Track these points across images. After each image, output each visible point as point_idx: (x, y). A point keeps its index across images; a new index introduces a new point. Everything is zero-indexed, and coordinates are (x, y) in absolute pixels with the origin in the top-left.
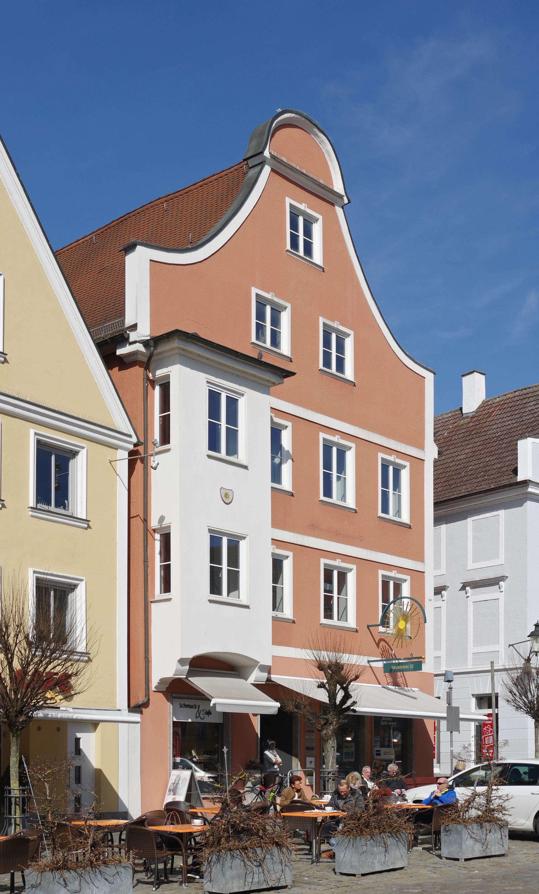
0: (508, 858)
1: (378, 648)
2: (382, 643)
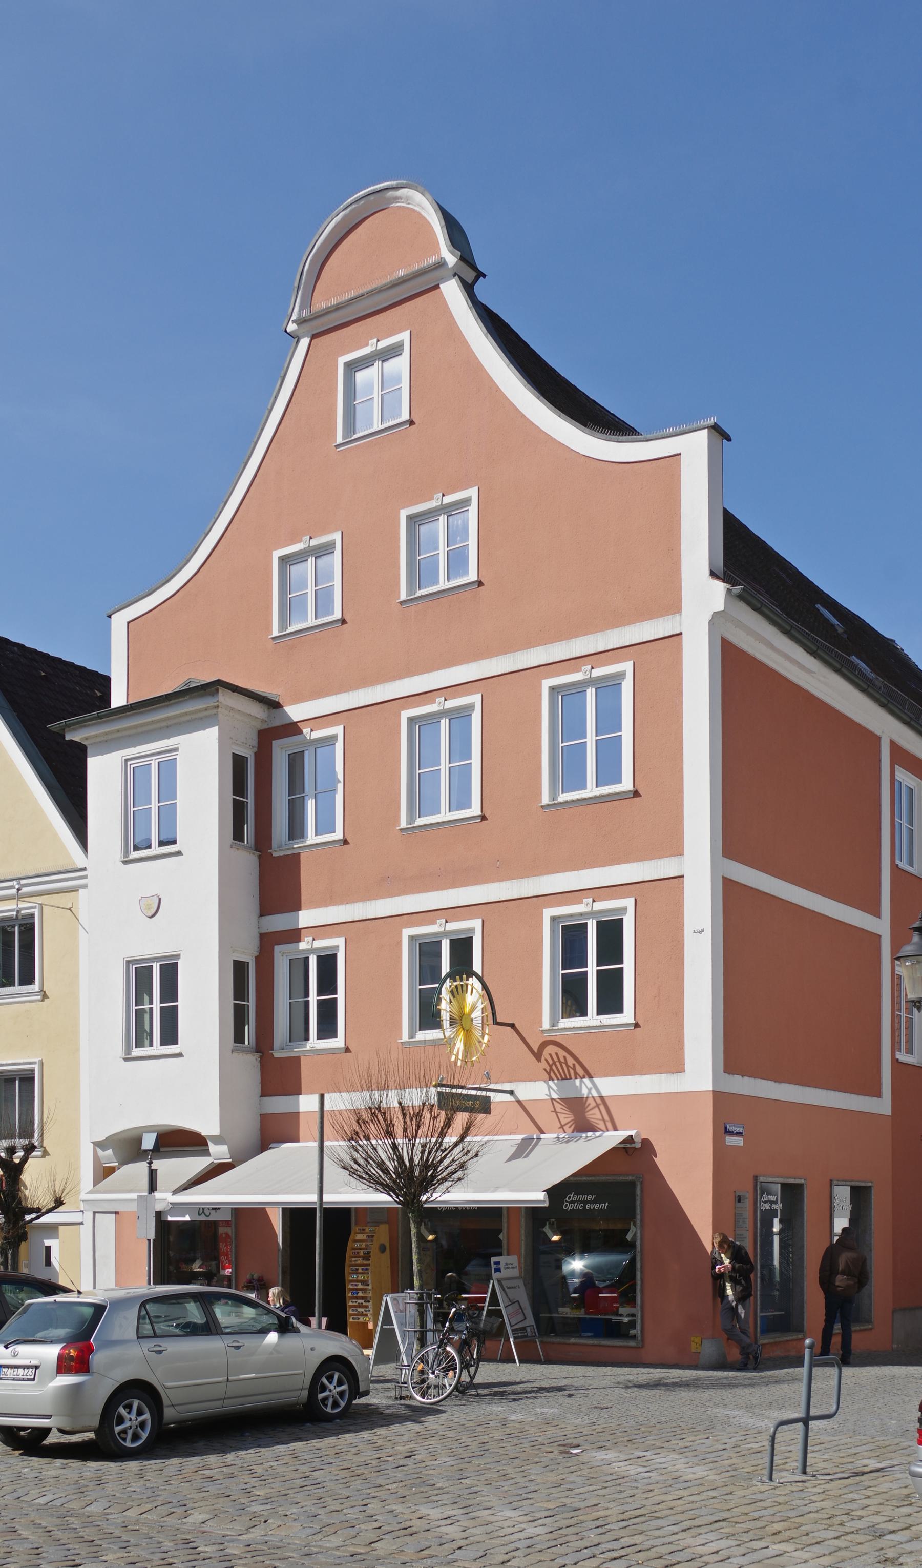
0: (443, 1416)
1: (539, 1060)
2: (551, 1049)
